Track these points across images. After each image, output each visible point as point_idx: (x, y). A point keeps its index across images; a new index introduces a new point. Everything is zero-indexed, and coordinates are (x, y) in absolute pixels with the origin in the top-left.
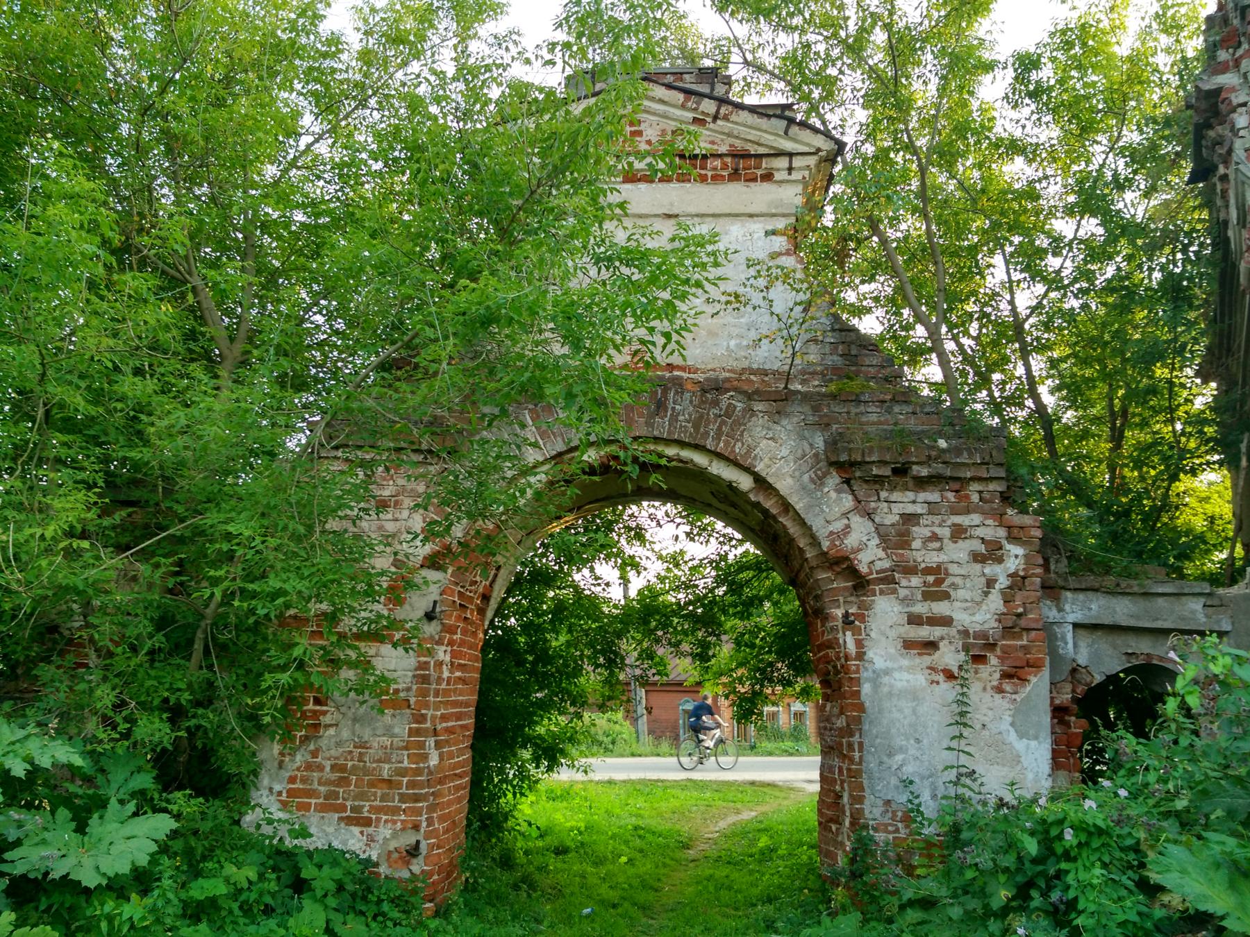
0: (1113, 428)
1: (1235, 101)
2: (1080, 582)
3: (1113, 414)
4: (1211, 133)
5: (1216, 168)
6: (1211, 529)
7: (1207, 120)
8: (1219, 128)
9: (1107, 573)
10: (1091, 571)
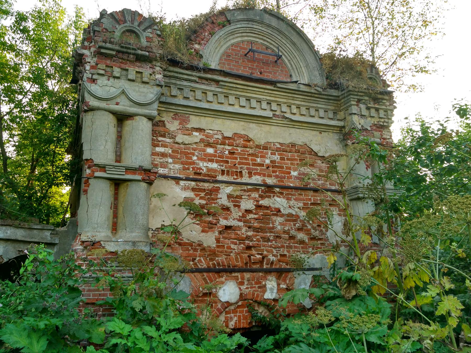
0: (32, 165)
1: (87, 60)
2: (4, 222)
3: (33, 159)
4: (79, 68)
5: (79, 81)
6: (61, 206)
7: (78, 63)
8: (81, 67)
9: (17, 219)
10: (10, 218)
